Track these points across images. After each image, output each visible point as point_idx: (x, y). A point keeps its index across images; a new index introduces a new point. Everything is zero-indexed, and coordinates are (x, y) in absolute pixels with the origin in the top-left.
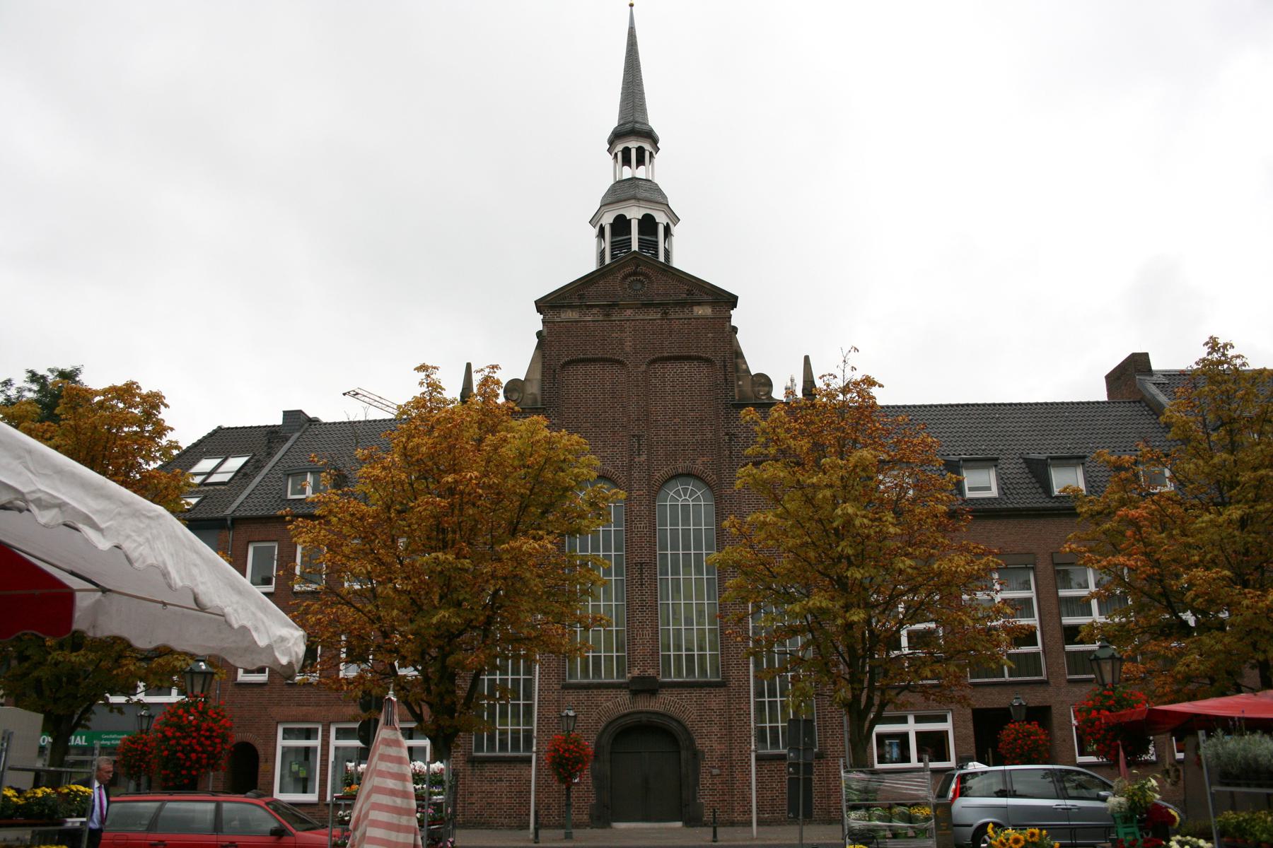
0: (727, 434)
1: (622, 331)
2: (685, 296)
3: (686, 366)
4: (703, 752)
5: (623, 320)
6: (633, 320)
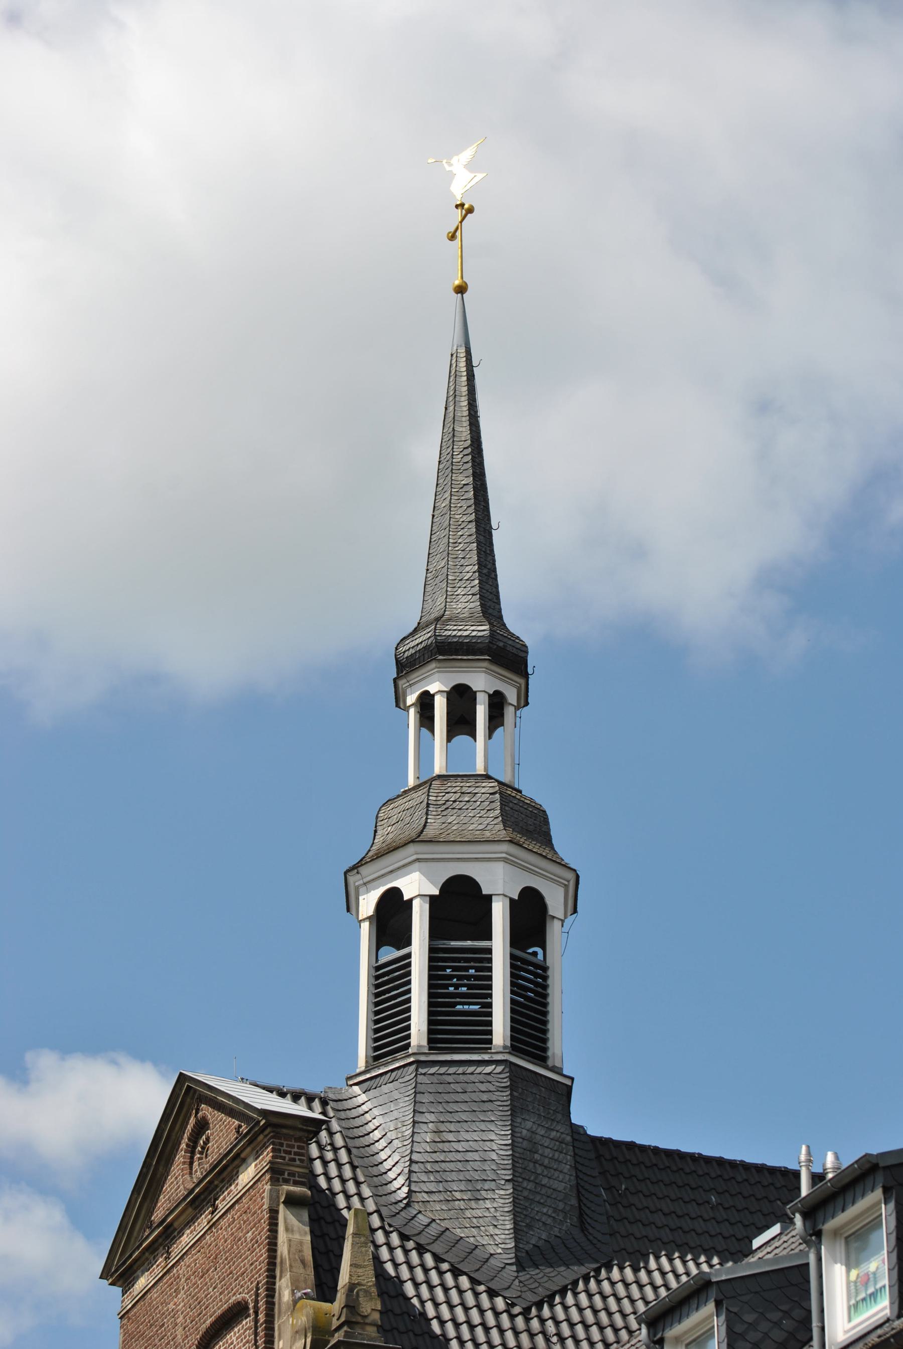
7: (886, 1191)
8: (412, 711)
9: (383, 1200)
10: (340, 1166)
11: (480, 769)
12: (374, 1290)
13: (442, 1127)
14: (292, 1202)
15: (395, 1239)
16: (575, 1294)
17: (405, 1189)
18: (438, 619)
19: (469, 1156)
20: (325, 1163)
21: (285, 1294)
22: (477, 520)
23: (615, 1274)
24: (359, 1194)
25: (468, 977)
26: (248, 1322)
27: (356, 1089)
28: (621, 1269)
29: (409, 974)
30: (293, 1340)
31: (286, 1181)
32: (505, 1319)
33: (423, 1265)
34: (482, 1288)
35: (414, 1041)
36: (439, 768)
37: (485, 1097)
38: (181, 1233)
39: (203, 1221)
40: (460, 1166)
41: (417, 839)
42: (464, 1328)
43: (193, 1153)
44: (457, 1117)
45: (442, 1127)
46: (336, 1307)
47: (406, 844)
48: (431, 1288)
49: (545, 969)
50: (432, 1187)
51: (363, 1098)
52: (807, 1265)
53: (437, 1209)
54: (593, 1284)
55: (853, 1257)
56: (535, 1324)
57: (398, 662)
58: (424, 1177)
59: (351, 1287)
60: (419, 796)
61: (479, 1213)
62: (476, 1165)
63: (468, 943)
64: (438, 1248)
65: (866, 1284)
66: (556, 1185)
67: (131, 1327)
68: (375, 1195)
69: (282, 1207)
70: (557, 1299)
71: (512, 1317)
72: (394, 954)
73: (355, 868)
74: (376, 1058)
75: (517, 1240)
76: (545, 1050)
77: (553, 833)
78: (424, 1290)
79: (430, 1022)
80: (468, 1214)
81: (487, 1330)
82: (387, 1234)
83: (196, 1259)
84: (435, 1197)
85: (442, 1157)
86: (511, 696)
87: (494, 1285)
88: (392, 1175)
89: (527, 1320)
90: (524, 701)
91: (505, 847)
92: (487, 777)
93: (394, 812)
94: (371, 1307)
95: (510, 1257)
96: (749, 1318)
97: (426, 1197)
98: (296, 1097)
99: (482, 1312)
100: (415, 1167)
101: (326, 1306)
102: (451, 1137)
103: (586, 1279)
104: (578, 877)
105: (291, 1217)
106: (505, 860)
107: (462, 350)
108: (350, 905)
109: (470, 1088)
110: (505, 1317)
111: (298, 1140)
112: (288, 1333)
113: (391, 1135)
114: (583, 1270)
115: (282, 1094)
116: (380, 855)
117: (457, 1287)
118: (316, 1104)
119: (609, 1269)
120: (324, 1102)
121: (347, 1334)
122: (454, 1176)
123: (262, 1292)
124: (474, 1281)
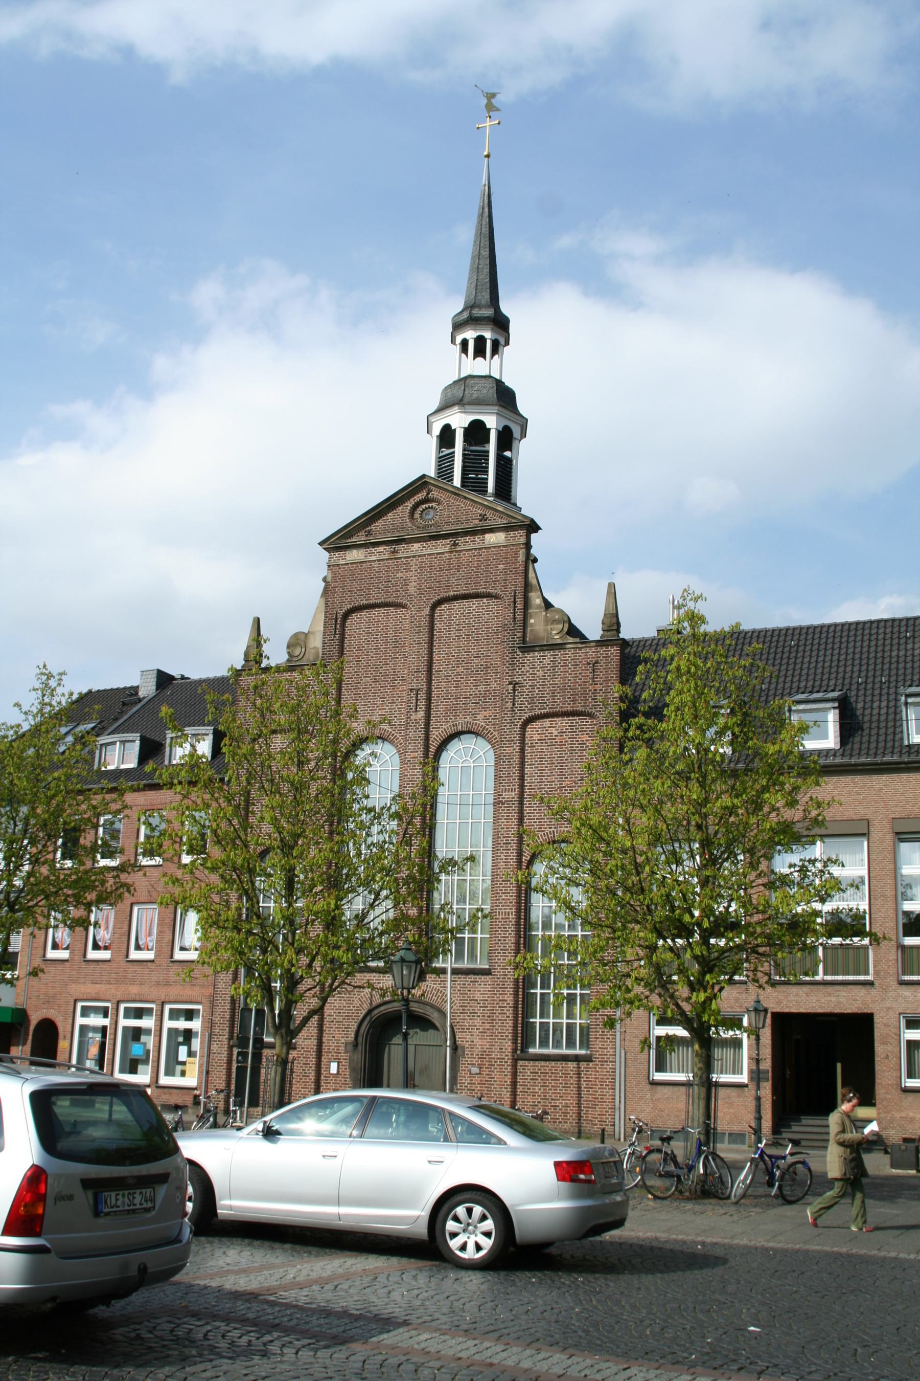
0: (510, 683)
1: (408, 570)
2: (477, 522)
3: (474, 604)
4: (463, 1047)
5: (409, 557)
6: (420, 556)
86: (502, 341)
90: (507, 343)
91: (497, 408)
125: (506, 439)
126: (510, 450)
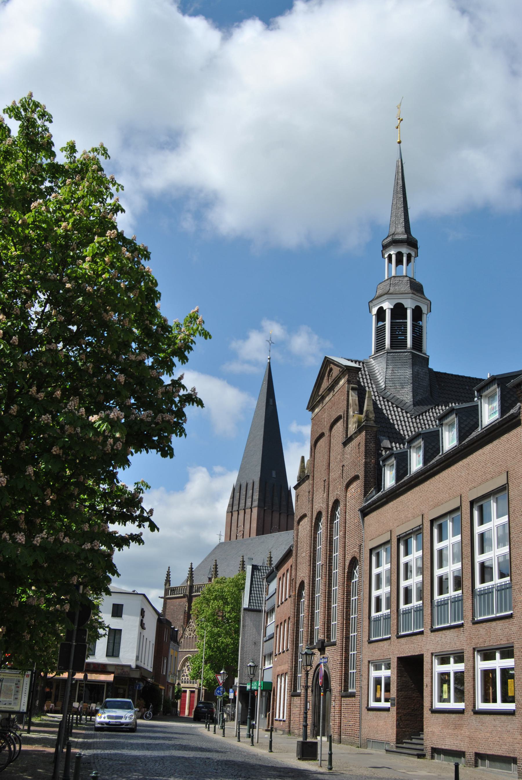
7: (498, 385)
8: (386, 259)
9: (378, 388)
10: (367, 380)
11: (404, 274)
12: (373, 412)
13: (394, 369)
14: (353, 389)
15: (381, 398)
16: (429, 413)
17: (384, 386)
18: (393, 234)
19: (401, 377)
20: (363, 379)
21: (351, 413)
22: (404, 207)
23: (440, 408)
24: (372, 387)
25: (402, 330)
26: (342, 420)
27: (372, 360)
28: (442, 406)
29: (385, 329)
30: (353, 425)
31: (352, 384)
32: (410, 420)
33: (388, 405)
34: (404, 411)
35: (386, 347)
36: (393, 274)
37: (405, 361)
38: (326, 397)
39: (331, 394)
40: (398, 379)
41: (387, 293)
42: (399, 421)
43: (329, 377)
44: (397, 367)
45: (394, 369)
46: (363, 416)
47: (384, 295)
48: (390, 411)
49: (422, 327)
50: (391, 385)
51: (373, 362)
52: (478, 405)
53: (393, 390)
54: (434, 410)
55: (490, 402)
56: (418, 420)
57: (383, 246)
58: (389, 382)
59: (367, 411)
60: (388, 282)
61: (403, 392)
62: (403, 379)
63: (401, 321)
64: (393, 401)
65: (493, 409)
66: (424, 384)
67: (314, 422)
68: (376, 387)
69: (350, 391)
70: (424, 414)
71: (412, 419)
72: (382, 324)
73: (371, 301)
74: (377, 351)
75: (413, 398)
76: (422, 348)
77: (424, 291)
78: (389, 412)
79: (391, 342)
80: (401, 392)
81: (405, 422)
82: (379, 397)
83: (330, 403)
84: (392, 388)
85: (393, 377)
86: (413, 254)
87: (407, 410)
88: (380, 382)
89: (416, 420)
90: (417, 255)
91: (411, 295)
92: (406, 276)
93: (381, 286)
94: (372, 416)
95: (412, 403)
96: (464, 418)
97: (389, 387)
98: (356, 362)
99: (404, 417)
100: (387, 380)
101: (361, 416)
102: (396, 372)
103: (432, 409)
104: (431, 303)
105: (353, 394)
106: (411, 298)
107: (400, 160)
108: (370, 312)
109: (401, 359)
110: (410, 419)
111: (355, 373)
112: (352, 423)
113: (380, 371)
114: (431, 407)
115: (352, 361)
116: (378, 298)
117: (397, 411)
118: (361, 364)
119: (438, 406)
120: (363, 363)
121: (366, 423)
122: (397, 382)
123: (345, 412)
124: (402, 409)
125: (418, 314)
126: (421, 321)
